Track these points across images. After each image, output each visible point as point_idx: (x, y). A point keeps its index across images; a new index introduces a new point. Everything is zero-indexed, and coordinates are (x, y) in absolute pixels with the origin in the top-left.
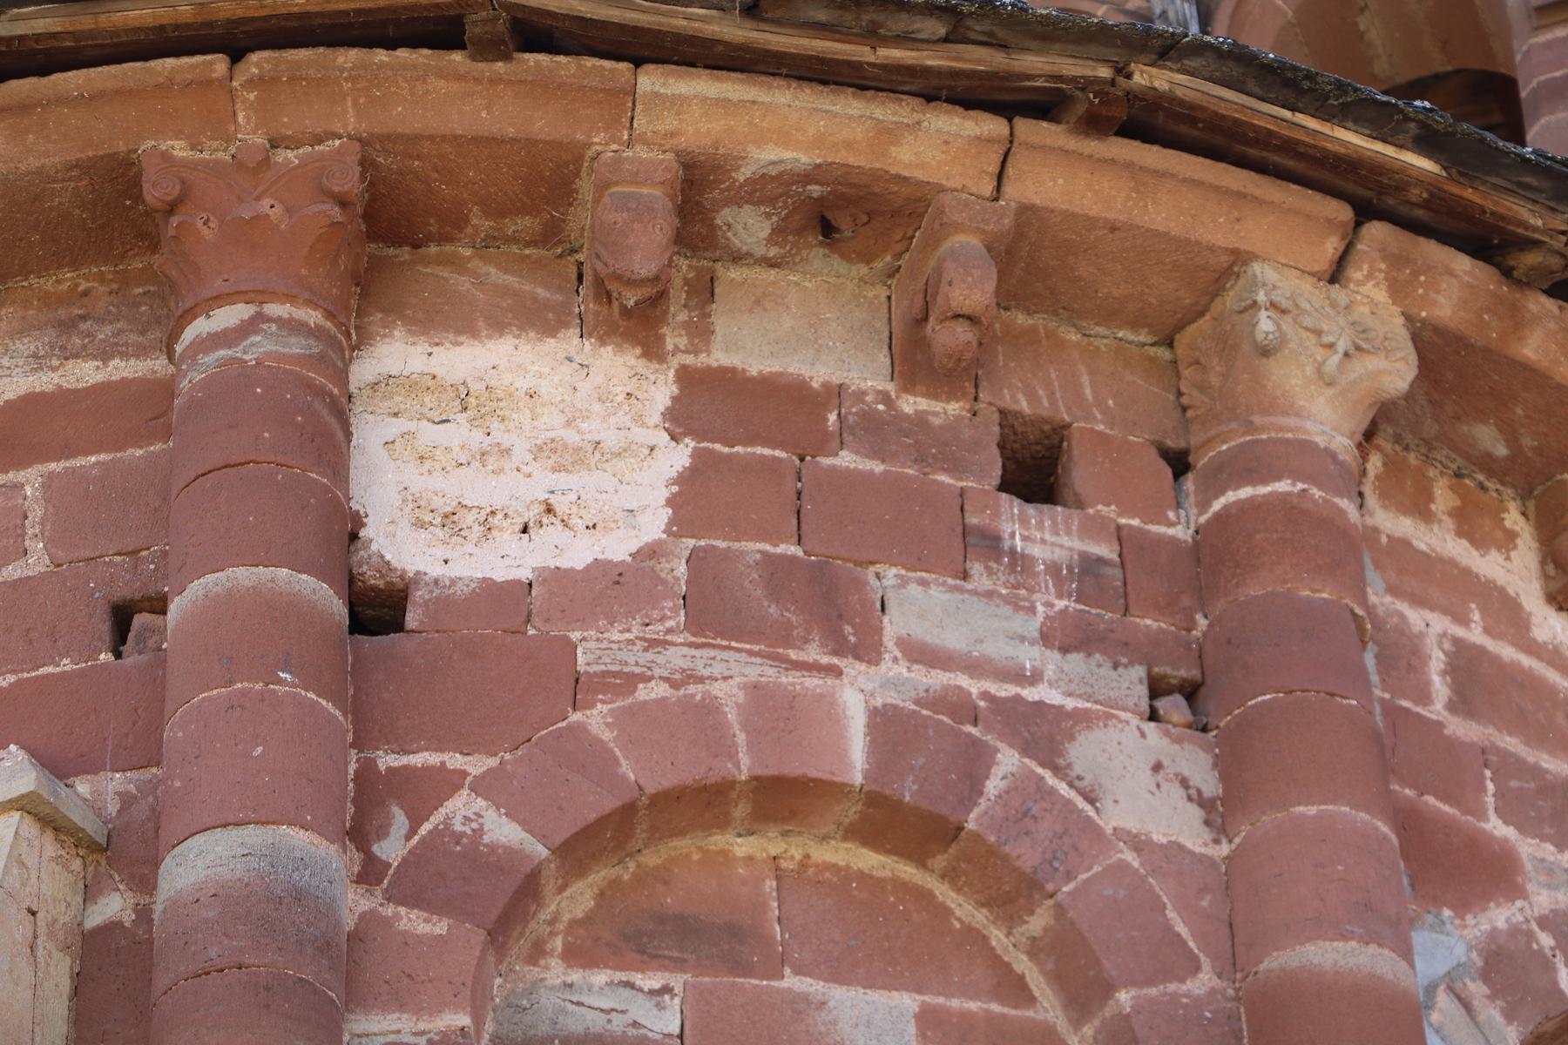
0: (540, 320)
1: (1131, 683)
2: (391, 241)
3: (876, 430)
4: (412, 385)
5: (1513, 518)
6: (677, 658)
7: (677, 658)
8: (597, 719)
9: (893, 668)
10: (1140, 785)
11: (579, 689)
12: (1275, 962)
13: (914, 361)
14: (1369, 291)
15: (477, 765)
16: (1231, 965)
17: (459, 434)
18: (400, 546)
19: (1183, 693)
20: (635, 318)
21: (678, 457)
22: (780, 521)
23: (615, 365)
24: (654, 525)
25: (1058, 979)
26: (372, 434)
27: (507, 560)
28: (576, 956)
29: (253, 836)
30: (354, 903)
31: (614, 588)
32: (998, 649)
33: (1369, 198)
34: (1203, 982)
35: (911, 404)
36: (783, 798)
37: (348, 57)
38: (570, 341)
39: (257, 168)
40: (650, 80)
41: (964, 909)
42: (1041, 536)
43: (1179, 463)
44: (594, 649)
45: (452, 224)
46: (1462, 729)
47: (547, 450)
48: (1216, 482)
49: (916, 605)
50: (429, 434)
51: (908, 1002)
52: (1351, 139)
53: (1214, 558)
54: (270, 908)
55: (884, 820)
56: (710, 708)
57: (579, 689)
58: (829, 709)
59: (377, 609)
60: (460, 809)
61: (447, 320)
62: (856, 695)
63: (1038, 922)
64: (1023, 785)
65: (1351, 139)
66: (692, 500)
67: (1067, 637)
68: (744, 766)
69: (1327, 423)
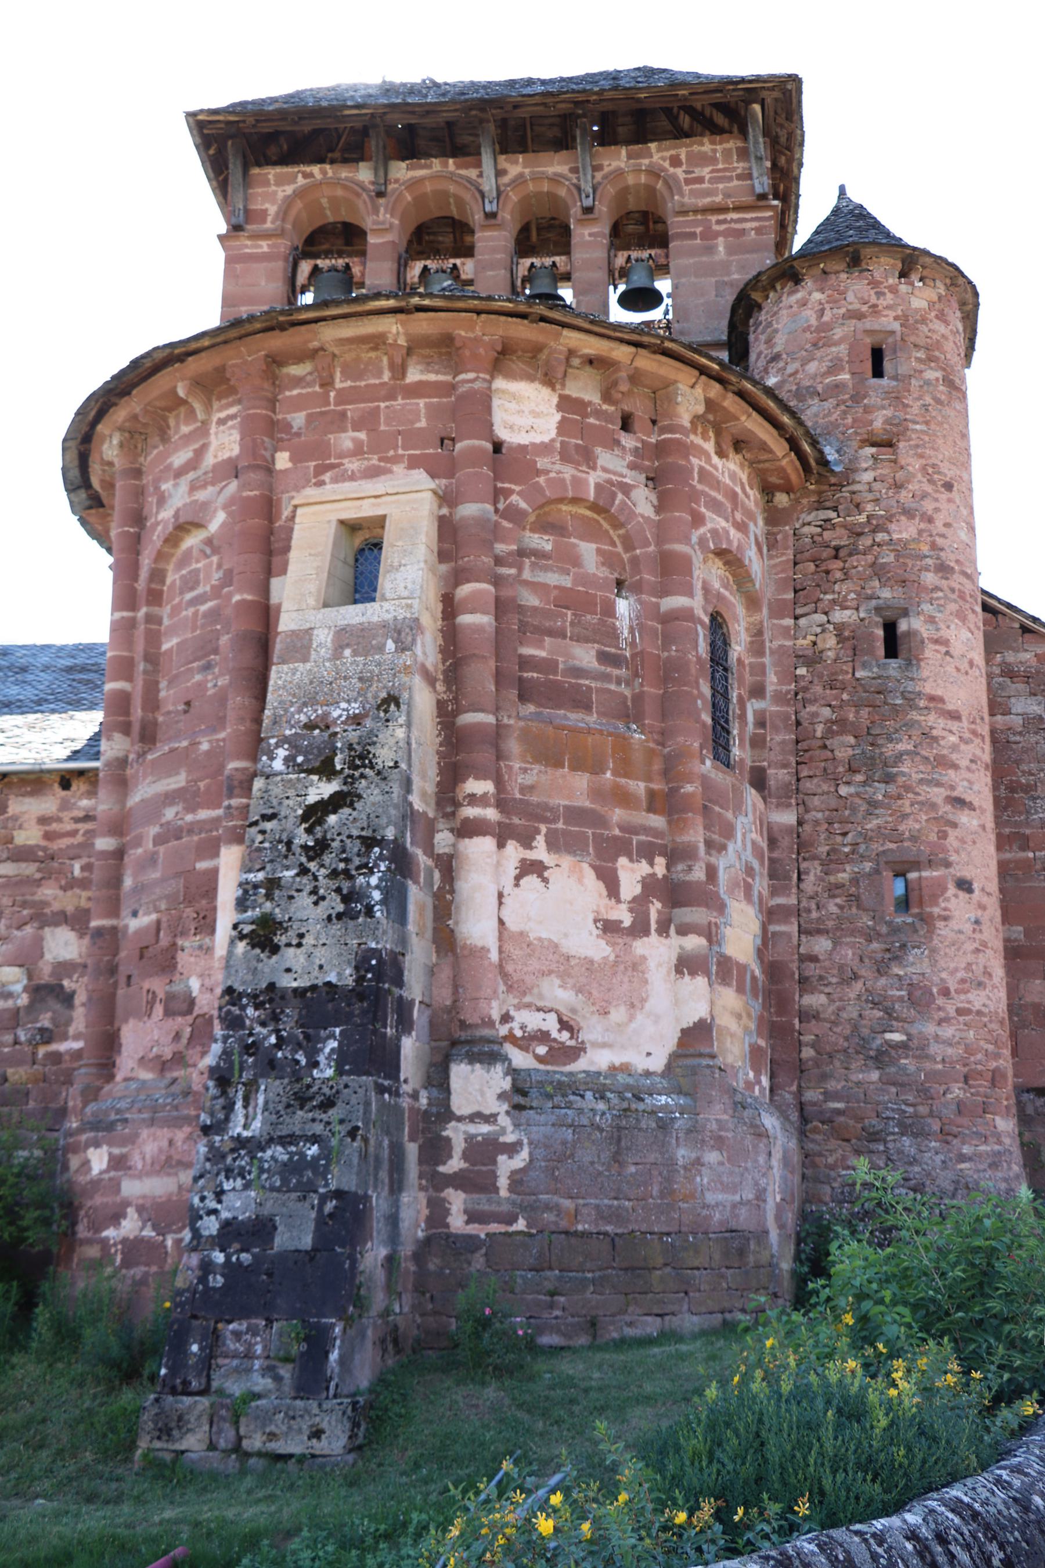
0: (531, 379)
1: (642, 478)
2: (503, 358)
3: (598, 413)
4: (504, 391)
5: (711, 434)
6: (557, 467)
7: (557, 467)
8: (541, 480)
9: (599, 473)
10: (643, 502)
11: (538, 473)
12: (667, 547)
13: (607, 397)
14: (699, 390)
15: (517, 488)
16: (657, 544)
17: (513, 406)
18: (502, 433)
19: (653, 480)
20: (549, 381)
21: (558, 417)
22: (579, 436)
23: (545, 392)
24: (553, 433)
25: (623, 543)
26: (496, 402)
27: (523, 439)
28: (532, 530)
29: (479, 506)
30: (495, 518)
31: (545, 448)
32: (619, 469)
33: (703, 371)
34: (652, 548)
35: (605, 407)
36: (575, 501)
37: (503, 318)
38: (537, 385)
39: (476, 340)
40: (566, 332)
41: (605, 525)
42: (628, 441)
43: (654, 422)
44: (542, 463)
45: (514, 352)
46: (699, 487)
47: (532, 412)
48: (663, 430)
49: (605, 458)
50: (507, 405)
51: (594, 546)
52: (704, 361)
53: (660, 449)
54: (481, 522)
55: (594, 507)
56: (563, 480)
57: (538, 473)
58: (586, 481)
59: (498, 447)
60: (514, 498)
61: (511, 376)
62: (593, 478)
63: (622, 532)
64: (623, 502)
65: (704, 361)
66: (563, 427)
67: (632, 466)
68: (570, 494)
69: (685, 420)
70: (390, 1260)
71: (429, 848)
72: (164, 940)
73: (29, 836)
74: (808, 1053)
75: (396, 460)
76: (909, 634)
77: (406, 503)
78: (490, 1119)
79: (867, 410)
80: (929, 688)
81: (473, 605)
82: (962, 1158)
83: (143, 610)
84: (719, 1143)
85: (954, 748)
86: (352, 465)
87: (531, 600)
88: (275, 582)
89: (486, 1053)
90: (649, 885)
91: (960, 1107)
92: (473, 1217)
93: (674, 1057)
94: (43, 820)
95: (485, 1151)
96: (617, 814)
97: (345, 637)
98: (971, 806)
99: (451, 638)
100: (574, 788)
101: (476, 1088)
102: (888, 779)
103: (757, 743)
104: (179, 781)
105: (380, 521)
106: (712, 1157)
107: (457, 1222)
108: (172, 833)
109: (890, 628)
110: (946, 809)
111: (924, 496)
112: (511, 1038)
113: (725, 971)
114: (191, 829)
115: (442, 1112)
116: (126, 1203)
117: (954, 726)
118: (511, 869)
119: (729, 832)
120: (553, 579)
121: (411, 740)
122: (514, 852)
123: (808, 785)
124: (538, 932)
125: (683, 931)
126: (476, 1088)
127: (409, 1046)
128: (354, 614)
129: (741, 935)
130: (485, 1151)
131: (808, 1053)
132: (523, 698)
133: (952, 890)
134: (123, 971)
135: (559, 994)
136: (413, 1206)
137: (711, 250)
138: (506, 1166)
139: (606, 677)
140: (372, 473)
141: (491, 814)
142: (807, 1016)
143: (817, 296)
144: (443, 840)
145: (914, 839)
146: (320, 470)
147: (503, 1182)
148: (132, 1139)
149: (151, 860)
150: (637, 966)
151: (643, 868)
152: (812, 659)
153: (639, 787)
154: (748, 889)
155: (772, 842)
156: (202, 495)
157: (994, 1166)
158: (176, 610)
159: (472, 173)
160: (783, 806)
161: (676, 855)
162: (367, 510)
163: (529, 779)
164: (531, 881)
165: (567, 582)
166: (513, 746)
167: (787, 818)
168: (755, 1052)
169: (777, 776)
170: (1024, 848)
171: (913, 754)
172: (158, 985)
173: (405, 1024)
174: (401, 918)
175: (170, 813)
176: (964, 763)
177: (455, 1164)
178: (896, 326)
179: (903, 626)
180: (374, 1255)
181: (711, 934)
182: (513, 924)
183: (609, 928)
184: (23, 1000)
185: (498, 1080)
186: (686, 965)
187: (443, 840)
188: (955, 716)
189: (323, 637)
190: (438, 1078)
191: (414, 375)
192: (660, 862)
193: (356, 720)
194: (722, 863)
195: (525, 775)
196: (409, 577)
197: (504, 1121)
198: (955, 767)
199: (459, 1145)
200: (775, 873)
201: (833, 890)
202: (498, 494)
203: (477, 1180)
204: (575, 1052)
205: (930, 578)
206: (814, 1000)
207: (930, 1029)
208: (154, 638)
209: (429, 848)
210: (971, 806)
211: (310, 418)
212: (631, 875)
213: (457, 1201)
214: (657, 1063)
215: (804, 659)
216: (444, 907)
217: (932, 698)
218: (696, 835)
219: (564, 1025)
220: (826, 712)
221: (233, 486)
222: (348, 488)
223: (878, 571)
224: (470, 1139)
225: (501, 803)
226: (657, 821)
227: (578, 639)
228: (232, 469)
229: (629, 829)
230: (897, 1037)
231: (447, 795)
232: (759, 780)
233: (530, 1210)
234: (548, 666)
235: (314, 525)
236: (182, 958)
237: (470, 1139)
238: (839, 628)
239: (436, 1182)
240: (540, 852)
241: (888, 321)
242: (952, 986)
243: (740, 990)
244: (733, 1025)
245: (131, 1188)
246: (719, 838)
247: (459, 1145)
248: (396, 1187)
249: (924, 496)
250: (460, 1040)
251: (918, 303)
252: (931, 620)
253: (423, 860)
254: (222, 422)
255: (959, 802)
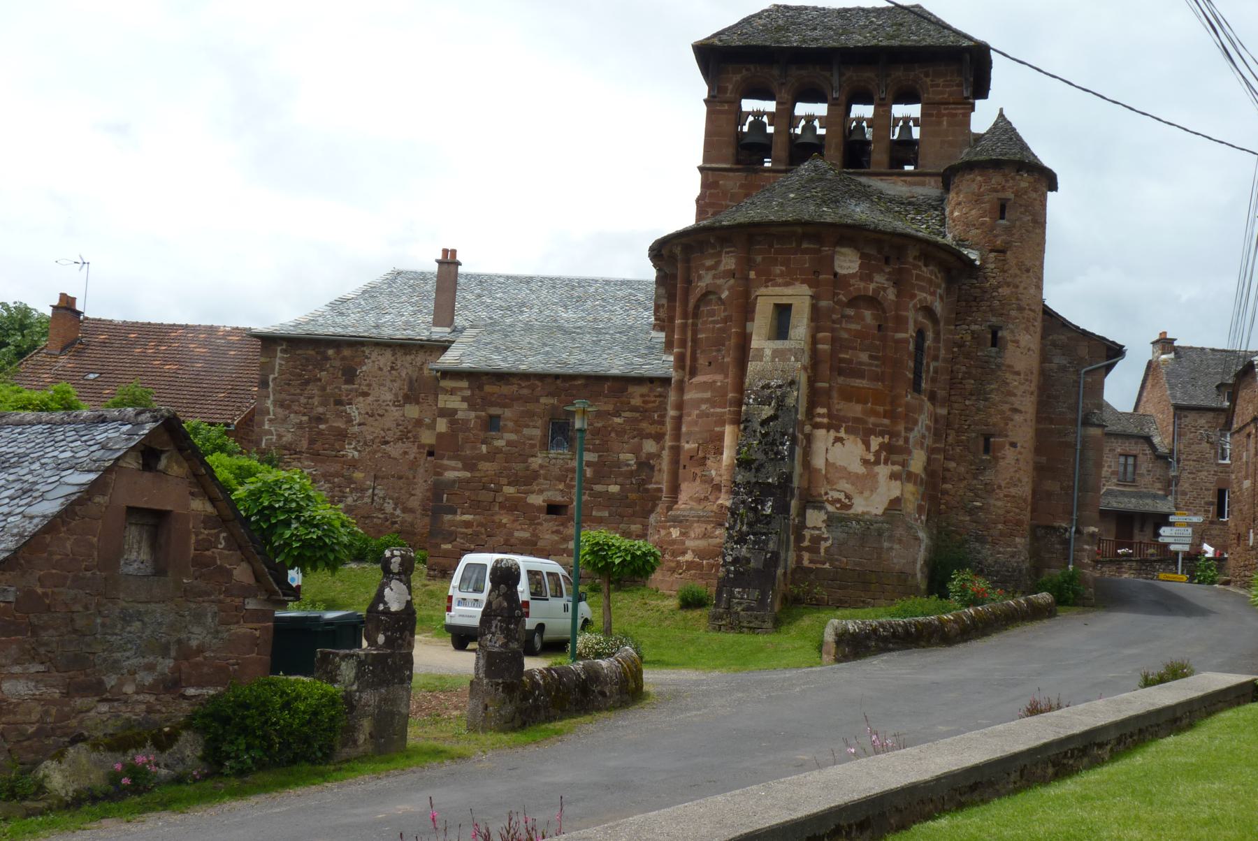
19: (896, 284)
22: (866, 274)
31: (853, 276)
44: (852, 281)
62: (872, 286)
66: (861, 266)
70: (785, 573)
71: (802, 432)
72: (701, 454)
73: (636, 401)
74: (943, 507)
75: (796, 280)
76: (1003, 338)
77: (799, 297)
78: (819, 529)
79: (996, 236)
80: (1008, 362)
81: (823, 342)
82: (999, 553)
83: (690, 321)
84: (900, 541)
85: (1016, 387)
86: (780, 280)
87: (845, 335)
88: (749, 324)
89: (819, 506)
90: (882, 446)
91: (1002, 534)
92: (811, 561)
93: (886, 509)
94: (642, 396)
95: (817, 540)
96: (872, 420)
97: (776, 353)
98: (1020, 412)
99: (814, 353)
100: (856, 410)
101: (815, 518)
102: (986, 400)
103: (934, 380)
104: (708, 395)
105: (790, 306)
106: (896, 546)
107: (806, 563)
108: (703, 415)
109: (994, 334)
110: (1008, 413)
111: (1016, 276)
112: (827, 500)
113: (910, 477)
114: (713, 414)
115: (802, 525)
116: (687, 549)
117: (1017, 377)
118: (831, 440)
119: (916, 422)
120: (853, 326)
121: (798, 397)
122: (832, 434)
123: (953, 398)
124: (839, 463)
125: (893, 463)
126: (815, 518)
127: (794, 503)
128: (779, 344)
129: (917, 462)
130: (817, 540)
131: (943, 507)
132: (840, 374)
133: (1007, 446)
134: (682, 463)
135: (847, 487)
136: (792, 556)
137: (939, 123)
138: (824, 545)
139: (871, 365)
140: (787, 284)
141: (825, 420)
142: (945, 492)
143: (979, 178)
144: (807, 428)
145: (994, 425)
146: (767, 281)
147: (822, 551)
148: (690, 527)
149: (696, 423)
150: (875, 476)
151: (880, 440)
152: (961, 345)
153: (881, 409)
154: (922, 444)
155: (936, 421)
156: (719, 282)
157: (1013, 557)
158: (705, 323)
159: (828, 74)
160: (942, 406)
161: (893, 435)
162: (785, 301)
163: (839, 407)
164: (838, 444)
165: (859, 327)
166: (835, 394)
167: (943, 411)
168: (920, 509)
169: (941, 393)
170: (1051, 423)
171: (997, 390)
172: (698, 470)
173: (792, 496)
174: (793, 460)
175: (704, 407)
176: (1019, 393)
177: (806, 543)
178: (1012, 196)
179: (1000, 334)
180: (780, 572)
181: (904, 464)
182: (831, 460)
183: (865, 462)
184: (634, 467)
185: (822, 516)
186: (894, 476)
187: (807, 428)
188: (1018, 373)
189: (768, 352)
190: (802, 514)
191: (805, 246)
192: (887, 437)
193: (780, 386)
194: (911, 436)
195: (840, 406)
196: (800, 329)
197: (824, 530)
198: (1015, 395)
199: (808, 537)
200: (937, 435)
201: (959, 443)
202: (835, 294)
203: (813, 549)
204: (850, 507)
205: (1013, 313)
206: (948, 486)
207: (992, 502)
208: (695, 333)
209: (802, 432)
210: (1020, 412)
211: (764, 259)
212: (875, 442)
213: (806, 556)
214: (880, 511)
215: (956, 344)
216: (807, 453)
217: (1009, 366)
218: (901, 427)
219: (847, 496)
220: (964, 369)
221: (732, 281)
222: (778, 290)
223: (992, 310)
224: (812, 535)
225: (829, 415)
226: (886, 421)
227: (862, 350)
228: (732, 274)
229: (875, 425)
230: (978, 504)
231: (810, 413)
232: (932, 397)
233: (831, 561)
234: (850, 361)
235: (765, 301)
236: (709, 462)
237: (812, 535)
238: (973, 332)
239: (799, 549)
240: (842, 434)
241: (1009, 195)
242: (1003, 484)
243: (915, 483)
244: (911, 498)
245: (689, 543)
246: (911, 424)
247: (808, 537)
248: (787, 551)
249: (1016, 276)
250: (811, 501)
251: (1024, 185)
252: (1012, 332)
253: (800, 436)
254: (727, 253)
255: (1016, 410)
